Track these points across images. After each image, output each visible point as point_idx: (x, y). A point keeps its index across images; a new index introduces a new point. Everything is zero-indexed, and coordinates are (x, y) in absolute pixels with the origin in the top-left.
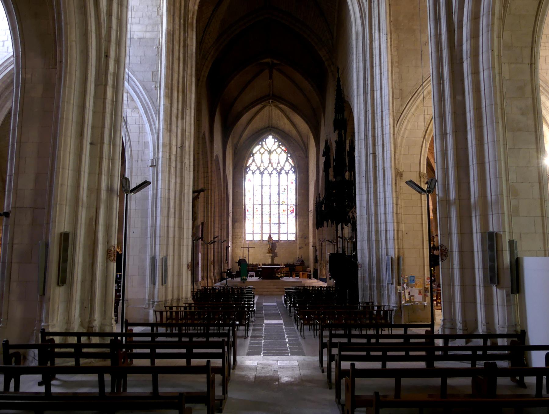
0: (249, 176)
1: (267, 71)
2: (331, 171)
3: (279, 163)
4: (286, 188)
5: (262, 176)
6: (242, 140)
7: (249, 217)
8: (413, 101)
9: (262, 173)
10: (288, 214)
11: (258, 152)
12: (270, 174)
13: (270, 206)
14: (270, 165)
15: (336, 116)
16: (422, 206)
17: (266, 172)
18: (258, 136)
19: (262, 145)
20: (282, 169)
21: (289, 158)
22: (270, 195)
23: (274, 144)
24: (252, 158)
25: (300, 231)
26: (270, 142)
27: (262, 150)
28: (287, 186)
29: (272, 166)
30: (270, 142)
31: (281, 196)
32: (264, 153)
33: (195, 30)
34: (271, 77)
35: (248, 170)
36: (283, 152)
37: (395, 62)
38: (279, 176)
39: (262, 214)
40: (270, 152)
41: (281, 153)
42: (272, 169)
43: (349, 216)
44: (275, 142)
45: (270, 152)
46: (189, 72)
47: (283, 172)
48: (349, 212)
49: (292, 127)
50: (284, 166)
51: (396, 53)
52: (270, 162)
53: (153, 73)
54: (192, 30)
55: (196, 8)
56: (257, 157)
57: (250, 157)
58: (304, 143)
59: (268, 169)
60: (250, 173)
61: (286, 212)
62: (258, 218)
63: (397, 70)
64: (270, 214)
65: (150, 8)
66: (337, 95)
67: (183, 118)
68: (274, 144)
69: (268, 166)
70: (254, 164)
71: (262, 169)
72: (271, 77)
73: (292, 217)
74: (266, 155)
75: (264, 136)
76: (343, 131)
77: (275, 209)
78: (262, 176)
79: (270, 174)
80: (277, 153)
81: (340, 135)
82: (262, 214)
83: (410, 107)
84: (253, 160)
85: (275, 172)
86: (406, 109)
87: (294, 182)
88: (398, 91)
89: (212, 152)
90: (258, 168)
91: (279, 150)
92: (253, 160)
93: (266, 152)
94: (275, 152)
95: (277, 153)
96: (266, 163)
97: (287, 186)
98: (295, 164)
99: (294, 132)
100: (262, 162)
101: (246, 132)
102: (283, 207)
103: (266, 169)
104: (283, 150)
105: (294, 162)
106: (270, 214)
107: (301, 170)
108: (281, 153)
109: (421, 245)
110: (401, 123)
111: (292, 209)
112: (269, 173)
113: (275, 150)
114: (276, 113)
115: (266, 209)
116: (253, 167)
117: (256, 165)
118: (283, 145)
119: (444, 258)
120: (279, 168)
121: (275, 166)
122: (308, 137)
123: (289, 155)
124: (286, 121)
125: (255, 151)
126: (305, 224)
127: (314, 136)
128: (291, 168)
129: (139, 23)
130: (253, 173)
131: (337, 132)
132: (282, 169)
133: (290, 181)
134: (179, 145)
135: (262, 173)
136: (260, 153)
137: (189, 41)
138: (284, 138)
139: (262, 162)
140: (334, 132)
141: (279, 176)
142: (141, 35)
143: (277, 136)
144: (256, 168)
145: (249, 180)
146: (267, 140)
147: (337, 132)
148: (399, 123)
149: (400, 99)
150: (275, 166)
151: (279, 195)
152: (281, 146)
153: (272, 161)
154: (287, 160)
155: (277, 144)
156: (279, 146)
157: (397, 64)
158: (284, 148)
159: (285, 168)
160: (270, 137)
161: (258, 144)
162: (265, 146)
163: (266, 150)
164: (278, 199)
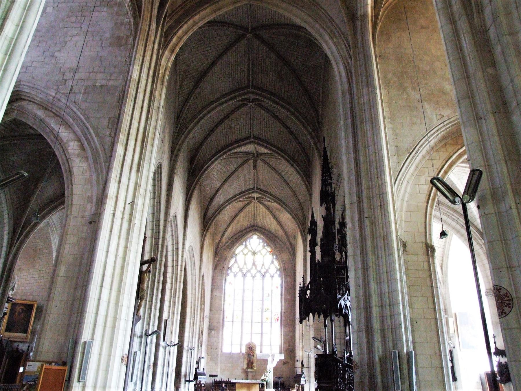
0: (230, 278)
1: (251, 161)
2: (318, 249)
3: (263, 265)
4: (270, 294)
5: (244, 279)
6: (224, 240)
7: (227, 324)
8: (410, 162)
9: (244, 275)
10: (271, 323)
11: (241, 253)
12: (254, 277)
13: (252, 313)
14: (254, 267)
15: (322, 189)
16: (432, 286)
17: (249, 275)
18: (240, 236)
19: (246, 246)
20: (267, 271)
21: (274, 260)
22: (253, 301)
23: (259, 244)
24: (234, 259)
25: (285, 343)
26: (255, 242)
27: (246, 251)
28: (272, 290)
29: (256, 268)
30: (255, 242)
31: (264, 302)
32: (247, 254)
33: (165, 84)
34: (255, 167)
35: (229, 271)
36: (268, 254)
37: (387, 118)
38: (263, 280)
39: (242, 322)
40: (254, 253)
41: (266, 255)
42: (256, 271)
43: (341, 304)
44: (260, 242)
45: (254, 253)
46: (153, 124)
47: (268, 275)
48: (340, 298)
49: (278, 226)
50: (269, 268)
51: (388, 109)
52: (254, 264)
53: (109, 120)
54: (163, 85)
55: (170, 65)
56: (240, 258)
57: (232, 257)
58: (291, 244)
59: (252, 271)
60: (231, 275)
61: (269, 321)
62: (237, 325)
63: (391, 126)
64: (252, 322)
65: (119, 58)
66: (324, 161)
67: (138, 171)
68: (259, 244)
69: (252, 268)
70: (236, 265)
71: (245, 271)
72: (255, 167)
73: (277, 326)
74: (250, 256)
75: (249, 235)
76: (331, 205)
77: (257, 318)
78: (244, 279)
79: (254, 277)
80: (261, 254)
81: (328, 209)
82: (242, 322)
83: (408, 166)
84: (236, 261)
85: (259, 275)
86: (404, 168)
87: (280, 287)
88: (394, 147)
89: (168, 207)
90: (241, 270)
91: (264, 251)
92: (236, 261)
93: (250, 253)
94: (259, 254)
95: (261, 254)
96: (249, 265)
97: (272, 290)
98: (281, 267)
99: (280, 232)
100: (245, 263)
101: (230, 230)
102: (267, 314)
103: (249, 271)
104: (268, 251)
105: (280, 265)
106: (252, 322)
107: (288, 271)
108: (266, 255)
109: (435, 340)
110: (399, 182)
111: (276, 317)
112: (252, 276)
113: (260, 251)
114: (261, 209)
115: (247, 317)
116: (235, 269)
117: (239, 267)
118: (268, 245)
119: (507, 309)
120: (263, 271)
121: (259, 268)
122: (295, 238)
123: (275, 257)
124: (273, 220)
125: (237, 252)
126: (291, 334)
127: (302, 235)
128: (277, 271)
129: (104, 72)
130: (235, 276)
131: (324, 206)
132: (267, 271)
133: (275, 284)
134: (129, 200)
135: (244, 275)
136: (244, 254)
137: (157, 94)
138: (270, 237)
139: (245, 263)
140: (321, 205)
141: (263, 280)
142: (104, 82)
143: (262, 236)
144: (238, 269)
145: (230, 283)
146: (251, 240)
147: (324, 206)
148: (397, 182)
149: (396, 156)
150: (259, 268)
151: (263, 300)
152: (266, 247)
153: (256, 263)
154: (273, 262)
155: (262, 244)
156: (264, 246)
157: (390, 120)
158: (269, 249)
159: (269, 271)
160: (255, 237)
161: (242, 244)
162: (249, 247)
163: (249, 251)
164: (261, 306)
